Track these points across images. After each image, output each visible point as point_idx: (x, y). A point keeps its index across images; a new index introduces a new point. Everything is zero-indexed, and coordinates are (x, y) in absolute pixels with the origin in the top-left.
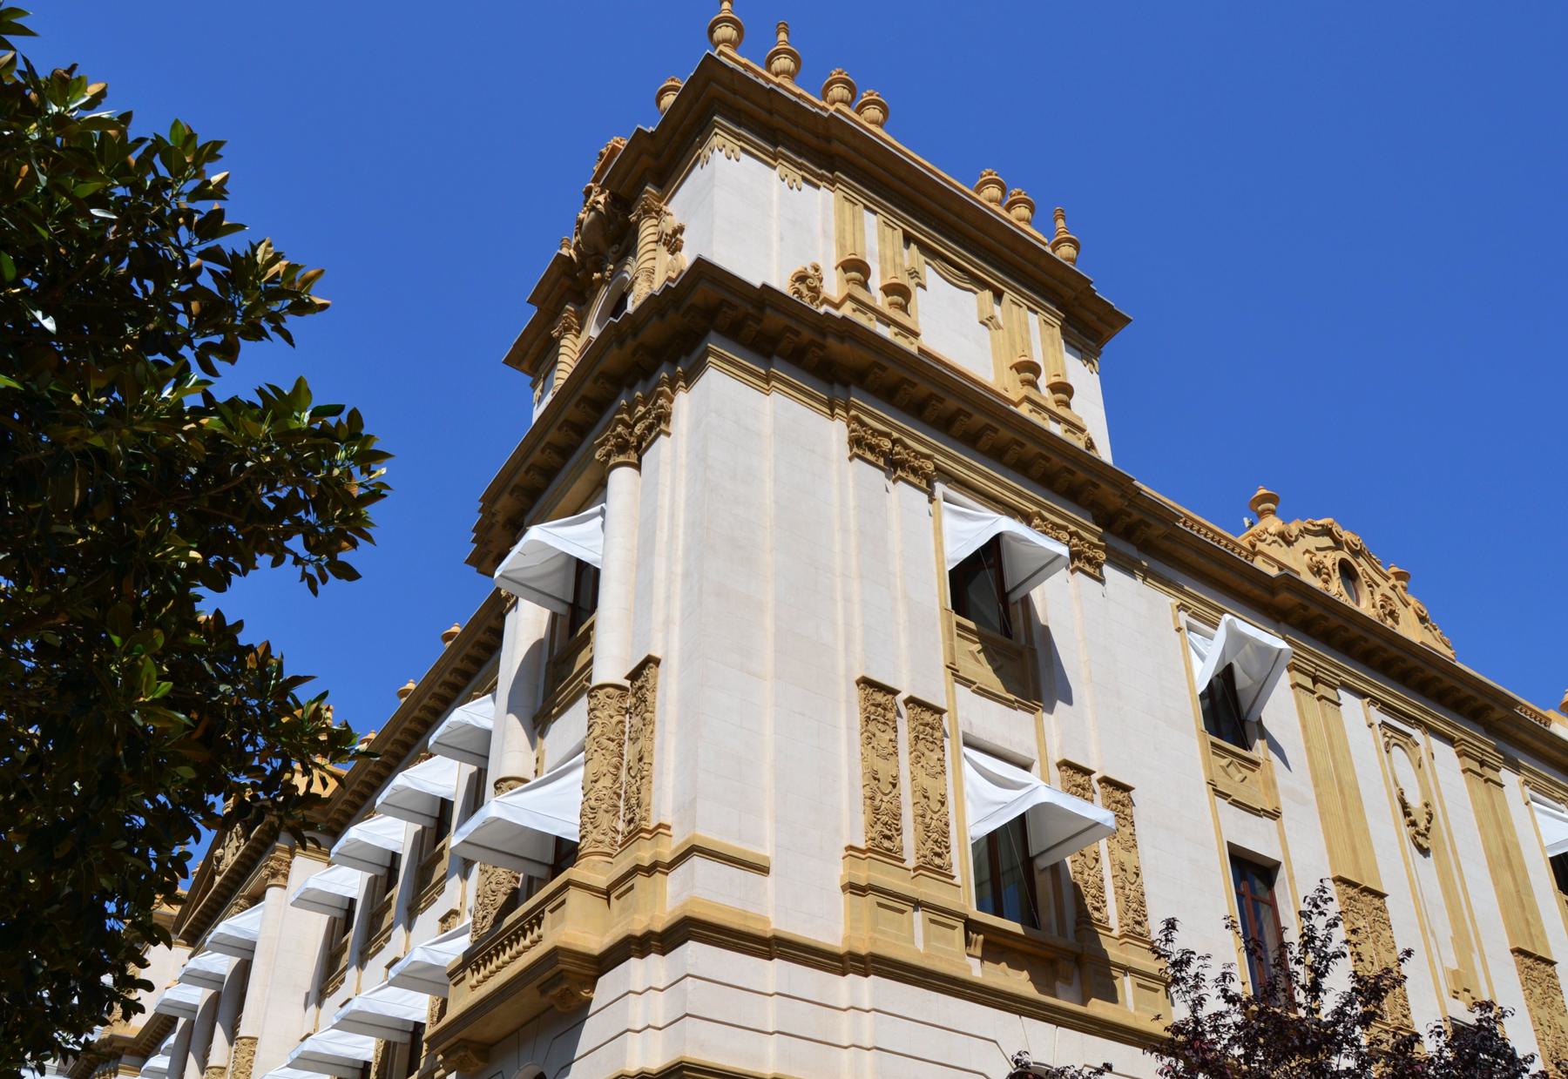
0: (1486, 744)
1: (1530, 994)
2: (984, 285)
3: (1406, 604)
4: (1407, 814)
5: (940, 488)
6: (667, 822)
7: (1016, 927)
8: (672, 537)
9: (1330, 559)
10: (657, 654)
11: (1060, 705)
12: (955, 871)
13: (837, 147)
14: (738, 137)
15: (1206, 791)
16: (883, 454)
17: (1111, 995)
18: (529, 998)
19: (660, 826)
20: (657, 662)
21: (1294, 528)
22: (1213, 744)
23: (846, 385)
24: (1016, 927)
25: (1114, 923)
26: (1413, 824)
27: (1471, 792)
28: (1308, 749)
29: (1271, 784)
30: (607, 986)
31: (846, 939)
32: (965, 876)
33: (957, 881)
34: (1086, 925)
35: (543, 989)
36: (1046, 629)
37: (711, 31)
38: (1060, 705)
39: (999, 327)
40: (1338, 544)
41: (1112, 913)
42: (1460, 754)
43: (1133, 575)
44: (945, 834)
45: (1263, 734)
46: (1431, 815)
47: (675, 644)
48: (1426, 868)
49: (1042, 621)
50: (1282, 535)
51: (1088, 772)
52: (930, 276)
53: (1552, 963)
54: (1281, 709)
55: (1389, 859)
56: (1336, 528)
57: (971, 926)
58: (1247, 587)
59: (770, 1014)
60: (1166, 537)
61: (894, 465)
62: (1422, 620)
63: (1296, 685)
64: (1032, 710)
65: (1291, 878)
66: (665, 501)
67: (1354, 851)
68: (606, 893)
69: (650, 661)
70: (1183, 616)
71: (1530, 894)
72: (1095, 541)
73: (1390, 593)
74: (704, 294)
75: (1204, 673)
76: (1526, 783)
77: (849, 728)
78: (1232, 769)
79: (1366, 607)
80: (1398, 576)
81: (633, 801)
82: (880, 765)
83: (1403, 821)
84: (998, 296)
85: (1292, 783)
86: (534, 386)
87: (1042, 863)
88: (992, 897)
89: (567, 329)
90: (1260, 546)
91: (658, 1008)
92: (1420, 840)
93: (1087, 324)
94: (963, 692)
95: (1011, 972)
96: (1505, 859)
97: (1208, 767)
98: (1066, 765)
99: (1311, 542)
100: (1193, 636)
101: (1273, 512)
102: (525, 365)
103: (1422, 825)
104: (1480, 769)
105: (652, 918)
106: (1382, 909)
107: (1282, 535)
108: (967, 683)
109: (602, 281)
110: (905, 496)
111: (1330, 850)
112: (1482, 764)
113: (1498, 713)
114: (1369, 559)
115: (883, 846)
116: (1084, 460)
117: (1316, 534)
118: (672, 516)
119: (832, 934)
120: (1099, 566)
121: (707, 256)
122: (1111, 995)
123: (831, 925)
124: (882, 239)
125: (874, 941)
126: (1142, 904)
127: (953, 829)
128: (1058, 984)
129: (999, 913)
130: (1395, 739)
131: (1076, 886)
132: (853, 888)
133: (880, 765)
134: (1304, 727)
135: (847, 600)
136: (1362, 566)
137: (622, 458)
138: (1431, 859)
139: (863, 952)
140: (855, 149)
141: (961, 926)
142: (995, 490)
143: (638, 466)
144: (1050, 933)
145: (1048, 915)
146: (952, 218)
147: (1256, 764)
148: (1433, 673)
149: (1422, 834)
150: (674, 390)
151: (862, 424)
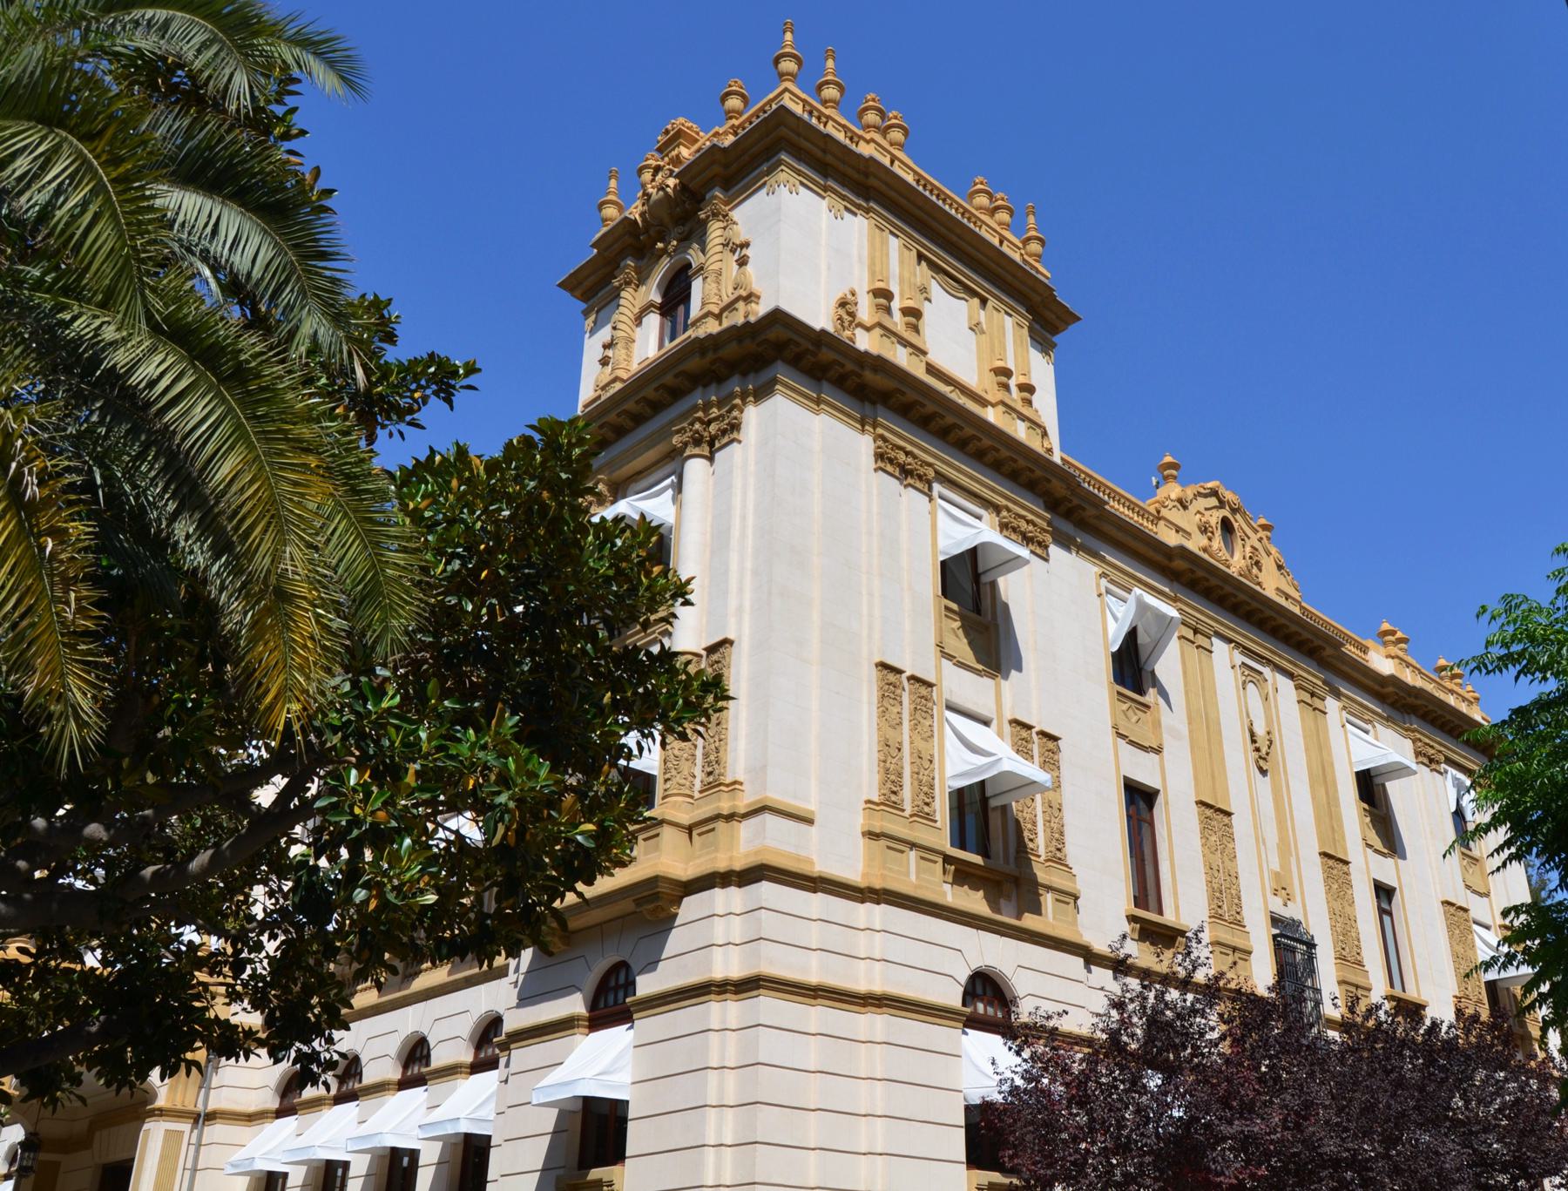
0: (1315, 677)
1: (1329, 890)
2: (974, 294)
3: (1269, 554)
4: (1254, 742)
5: (937, 487)
6: (741, 779)
7: (977, 859)
8: (743, 535)
9: (1214, 518)
10: (731, 636)
11: (1013, 673)
12: (938, 817)
13: (873, 182)
14: (799, 173)
15: (1110, 732)
16: (899, 465)
17: (1037, 909)
18: (627, 905)
19: (735, 783)
20: (731, 643)
21: (1189, 493)
22: (1119, 693)
23: (873, 403)
24: (977, 859)
25: (1042, 851)
26: (1258, 750)
27: (1303, 720)
28: (1187, 693)
29: (1157, 724)
30: (691, 907)
31: (865, 875)
32: (943, 818)
33: (938, 825)
34: (1022, 852)
35: (638, 902)
36: (1006, 607)
37: (777, 61)
38: (1013, 673)
39: (983, 332)
40: (1222, 504)
41: (1040, 844)
42: (1298, 687)
43: (1068, 549)
44: (932, 787)
45: (1155, 683)
46: (1271, 741)
47: (746, 630)
48: (1264, 784)
49: (1004, 598)
50: (1180, 501)
51: (1029, 727)
52: (936, 290)
53: (1346, 863)
54: (1169, 665)
55: (1240, 787)
56: (1222, 491)
57: (948, 859)
58: (1151, 554)
59: (814, 935)
60: (1097, 517)
61: (906, 473)
62: (1280, 567)
63: (1181, 637)
64: (993, 677)
65: (1167, 803)
66: (737, 501)
67: (1213, 777)
68: (689, 829)
69: (726, 642)
70: (1104, 582)
71: (1338, 805)
72: (1045, 525)
73: (1257, 545)
74: (774, 334)
75: (1115, 636)
76: (1344, 708)
77: (870, 703)
78: (1130, 713)
79: (1236, 564)
80: (1265, 527)
81: (712, 758)
82: (891, 733)
83: (1250, 747)
84: (984, 302)
85: (1173, 721)
86: (586, 314)
87: (993, 803)
88: (960, 841)
89: (628, 283)
90: (1164, 512)
91: (736, 929)
92: (1262, 763)
93: (1046, 319)
94: (946, 663)
95: (971, 893)
96: (1322, 777)
97: (1114, 715)
98: (1016, 722)
99: (1202, 503)
100: (1110, 599)
101: (1175, 477)
102: (578, 293)
103: (1264, 750)
104: (1311, 700)
105: (731, 858)
106: (1229, 826)
107: (1180, 501)
108: (950, 657)
109: (664, 251)
110: (912, 499)
111: (1196, 778)
112: (1313, 695)
113: (1329, 651)
114: (1244, 515)
115: (889, 802)
116: (1040, 462)
117: (1205, 496)
118: (744, 518)
119: (853, 874)
120: (1046, 547)
121: (787, 307)
122: (1037, 909)
123: (851, 864)
124: (901, 262)
125: (884, 877)
126: (1062, 834)
127: (937, 781)
128: (1002, 901)
129: (963, 847)
130: (1251, 676)
131: (1017, 822)
132: (872, 835)
133: (891, 733)
134: (1185, 673)
135: (871, 594)
136: (1238, 522)
137: (697, 451)
138: (1268, 779)
139: (877, 886)
140: (887, 184)
141: (940, 860)
142: (976, 487)
143: (711, 459)
144: (998, 863)
145: (997, 845)
146: (955, 239)
147: (1148, 707)
148: (1283, 621)
149: (1263, 756)
150: (744, 403)
151: (885, 440)
